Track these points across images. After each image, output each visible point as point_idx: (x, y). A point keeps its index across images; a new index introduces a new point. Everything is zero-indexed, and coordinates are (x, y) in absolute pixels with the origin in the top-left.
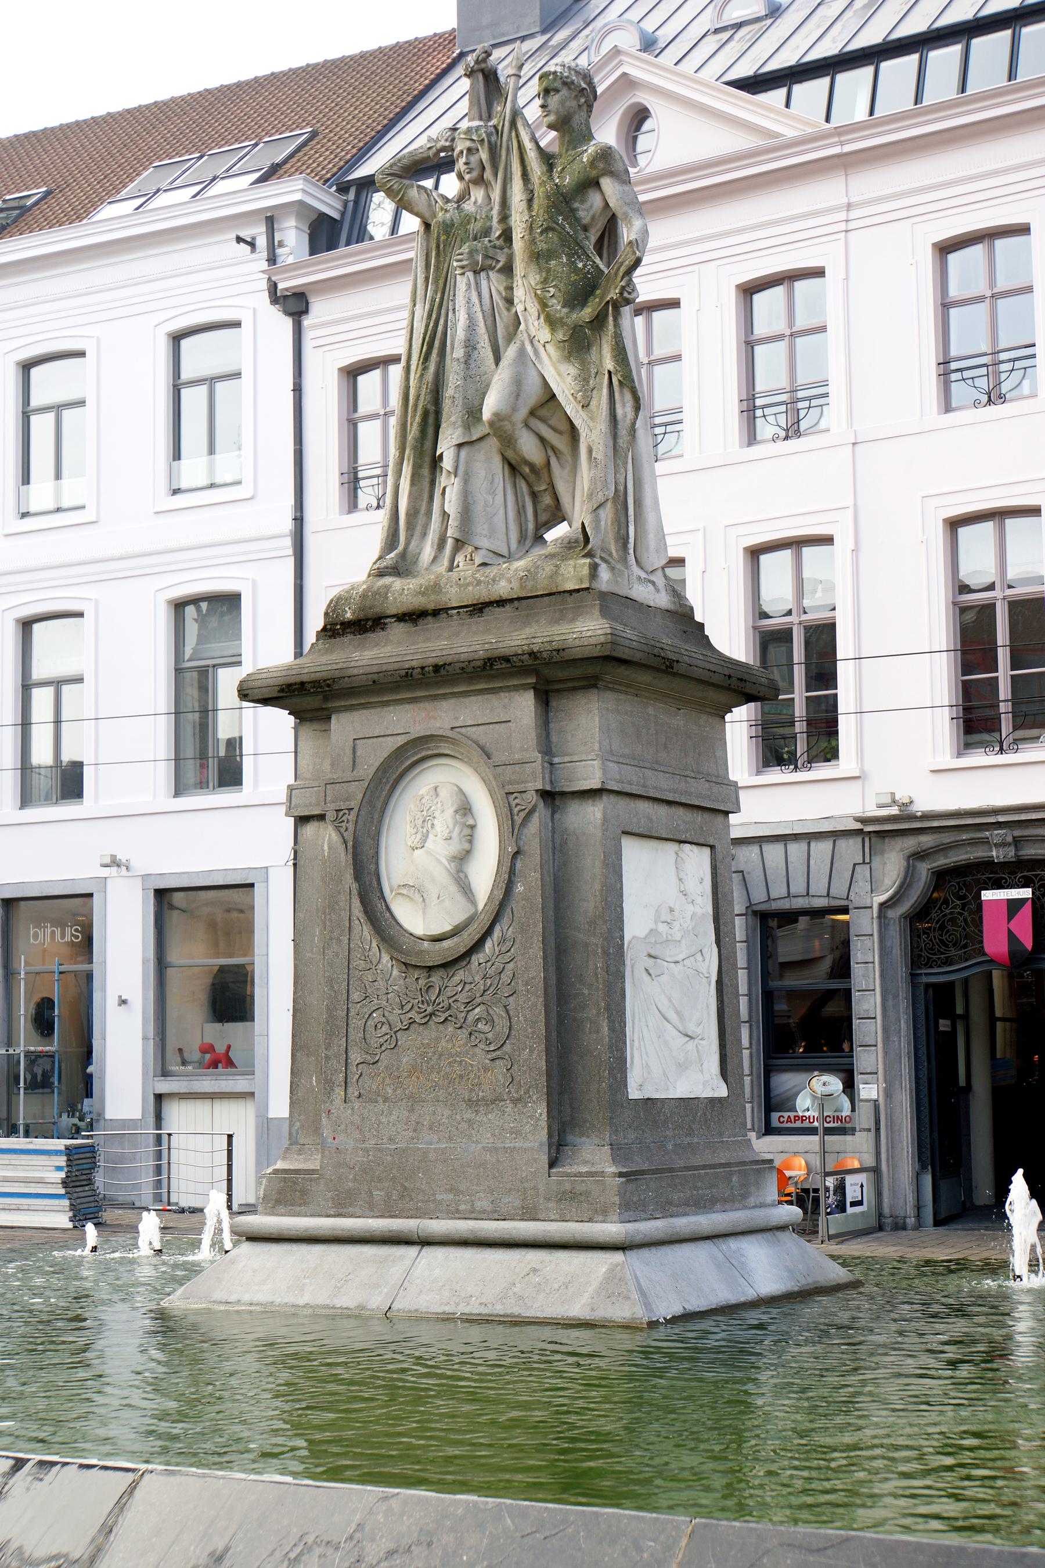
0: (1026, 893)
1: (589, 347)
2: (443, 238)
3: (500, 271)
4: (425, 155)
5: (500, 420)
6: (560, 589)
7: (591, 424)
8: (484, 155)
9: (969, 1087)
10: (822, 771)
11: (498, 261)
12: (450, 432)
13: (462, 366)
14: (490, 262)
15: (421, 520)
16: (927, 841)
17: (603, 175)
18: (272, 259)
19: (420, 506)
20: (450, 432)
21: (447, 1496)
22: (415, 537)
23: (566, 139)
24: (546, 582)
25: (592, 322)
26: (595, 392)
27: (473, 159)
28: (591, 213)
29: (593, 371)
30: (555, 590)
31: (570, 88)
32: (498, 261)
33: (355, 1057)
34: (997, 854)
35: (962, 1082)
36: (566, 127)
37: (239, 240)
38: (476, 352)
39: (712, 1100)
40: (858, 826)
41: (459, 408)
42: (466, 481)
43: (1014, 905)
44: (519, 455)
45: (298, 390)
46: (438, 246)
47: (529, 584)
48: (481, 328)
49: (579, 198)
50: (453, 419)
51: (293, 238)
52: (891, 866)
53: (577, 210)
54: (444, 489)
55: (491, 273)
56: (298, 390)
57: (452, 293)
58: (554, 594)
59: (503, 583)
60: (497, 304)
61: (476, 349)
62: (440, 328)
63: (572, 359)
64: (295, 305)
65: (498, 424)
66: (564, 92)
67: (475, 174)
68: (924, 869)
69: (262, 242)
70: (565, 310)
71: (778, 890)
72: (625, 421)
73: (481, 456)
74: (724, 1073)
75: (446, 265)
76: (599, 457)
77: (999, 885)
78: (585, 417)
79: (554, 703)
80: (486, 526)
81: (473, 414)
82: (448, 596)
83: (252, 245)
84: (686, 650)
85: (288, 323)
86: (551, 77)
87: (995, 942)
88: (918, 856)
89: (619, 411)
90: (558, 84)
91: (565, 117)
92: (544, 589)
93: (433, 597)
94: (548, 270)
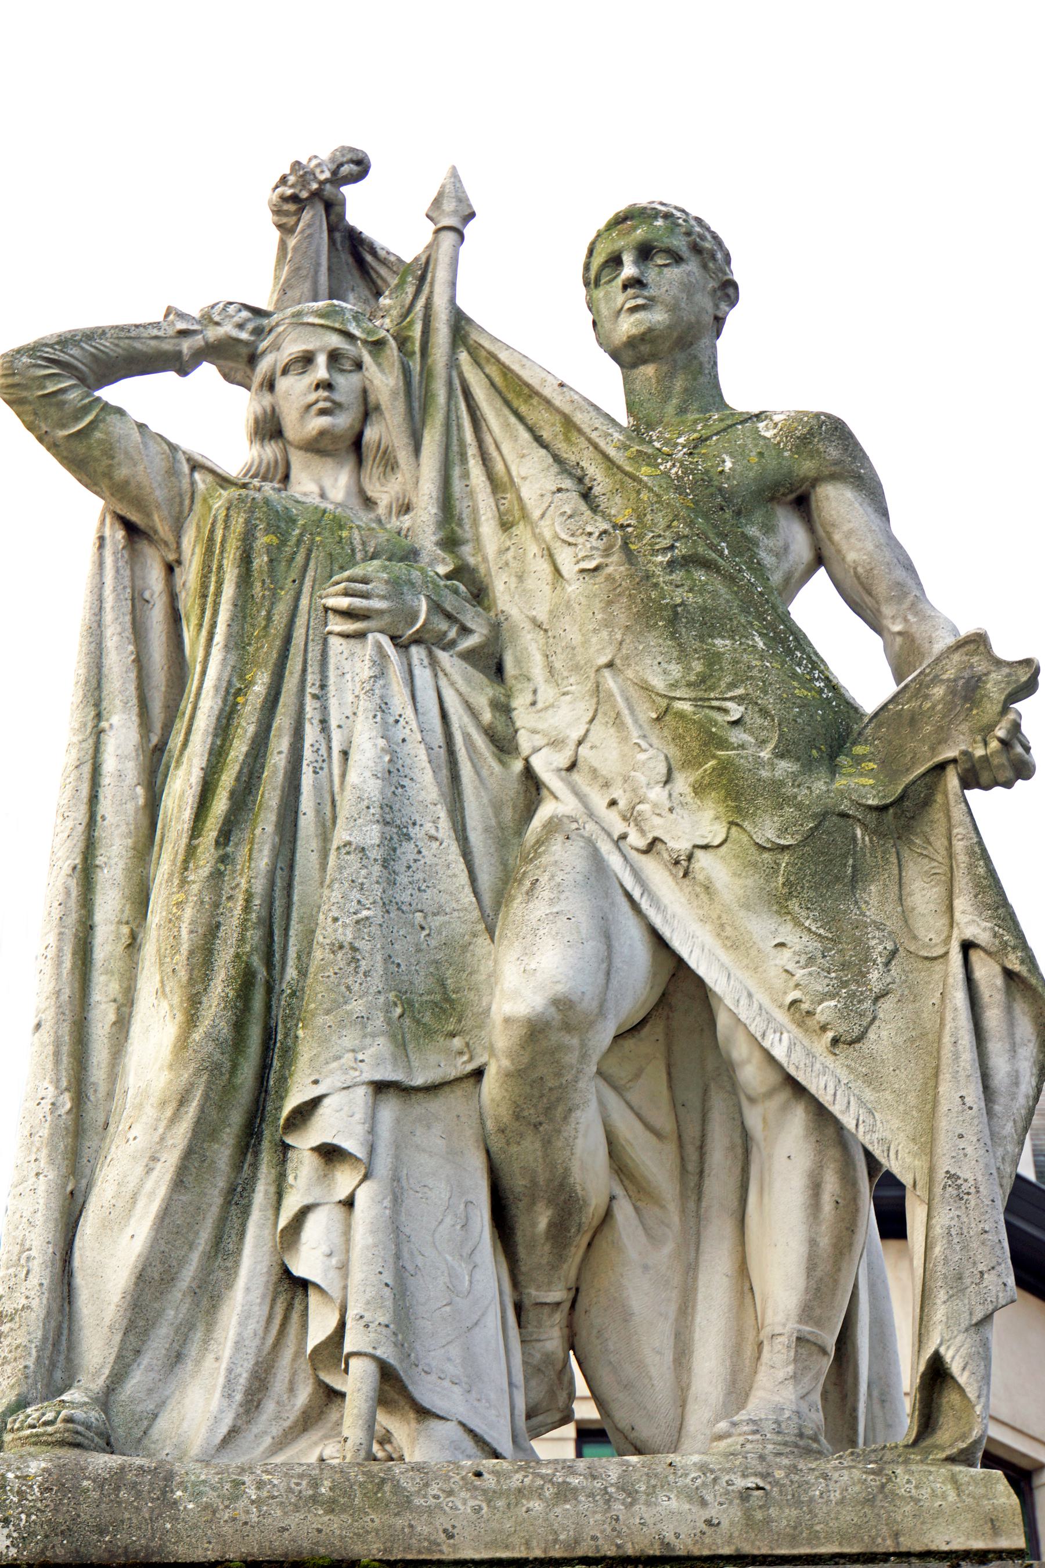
1: (856, 881)
2: (263, 540)
3: (468, 656)
4: (167, 346)
5: (567, 1027)
6: (907, 1544)
7: (868, 1095)
8: (383, 380)
11: (465, 631)
12: (348, 1042)
13: (377, 869)
14: (443, 625)
15: (175, 1307)
17: (833, 477)
19: (182, 1262)
20: (348, 1042)
22: (145, 1360)
23: (679, 384)
24: (849, 1516)
25: (882, 809)
26: (887, 1005)
27: (347, 384)
28: (785, 566)
29: (879, 949)
30: (888, 1545)
31: (705, 267)
32: (465, 631)
36: (681, 357)
38: (409, 847)
41: (376, 982)
42: (397, 1195)
44: (552, 1166)
46: (246, 560)
47: (783, 1517)
48: (426, 785)
49: (758, 516)
50: (357, 1006)
53: (753, 542)
54: (305, 1212)
55: (443, 656)
57: (312, 677)
58: (885, 1557)
59: (671, 1503)
60: (467, 737)
61: (408, 838)
62: (278, 759)
63: (794, 905)
65: (556, 1037)
66: (692, 266)
67: (343, 421)
70: (785, 767)
72: (1013, 1097)
73: (433, 1139)
75: (281, 610)
76: (965, 1173)
78: (844, 1076)
80: (454, 1351)
81: (431, 1004)
82: (442, 1522)
86: (659, 222)
89: (1000, 1065)
90: (679, 243)
91: (690, 327)
92: (843, 1537)
93: (375, 1519)
94: (713, 659)
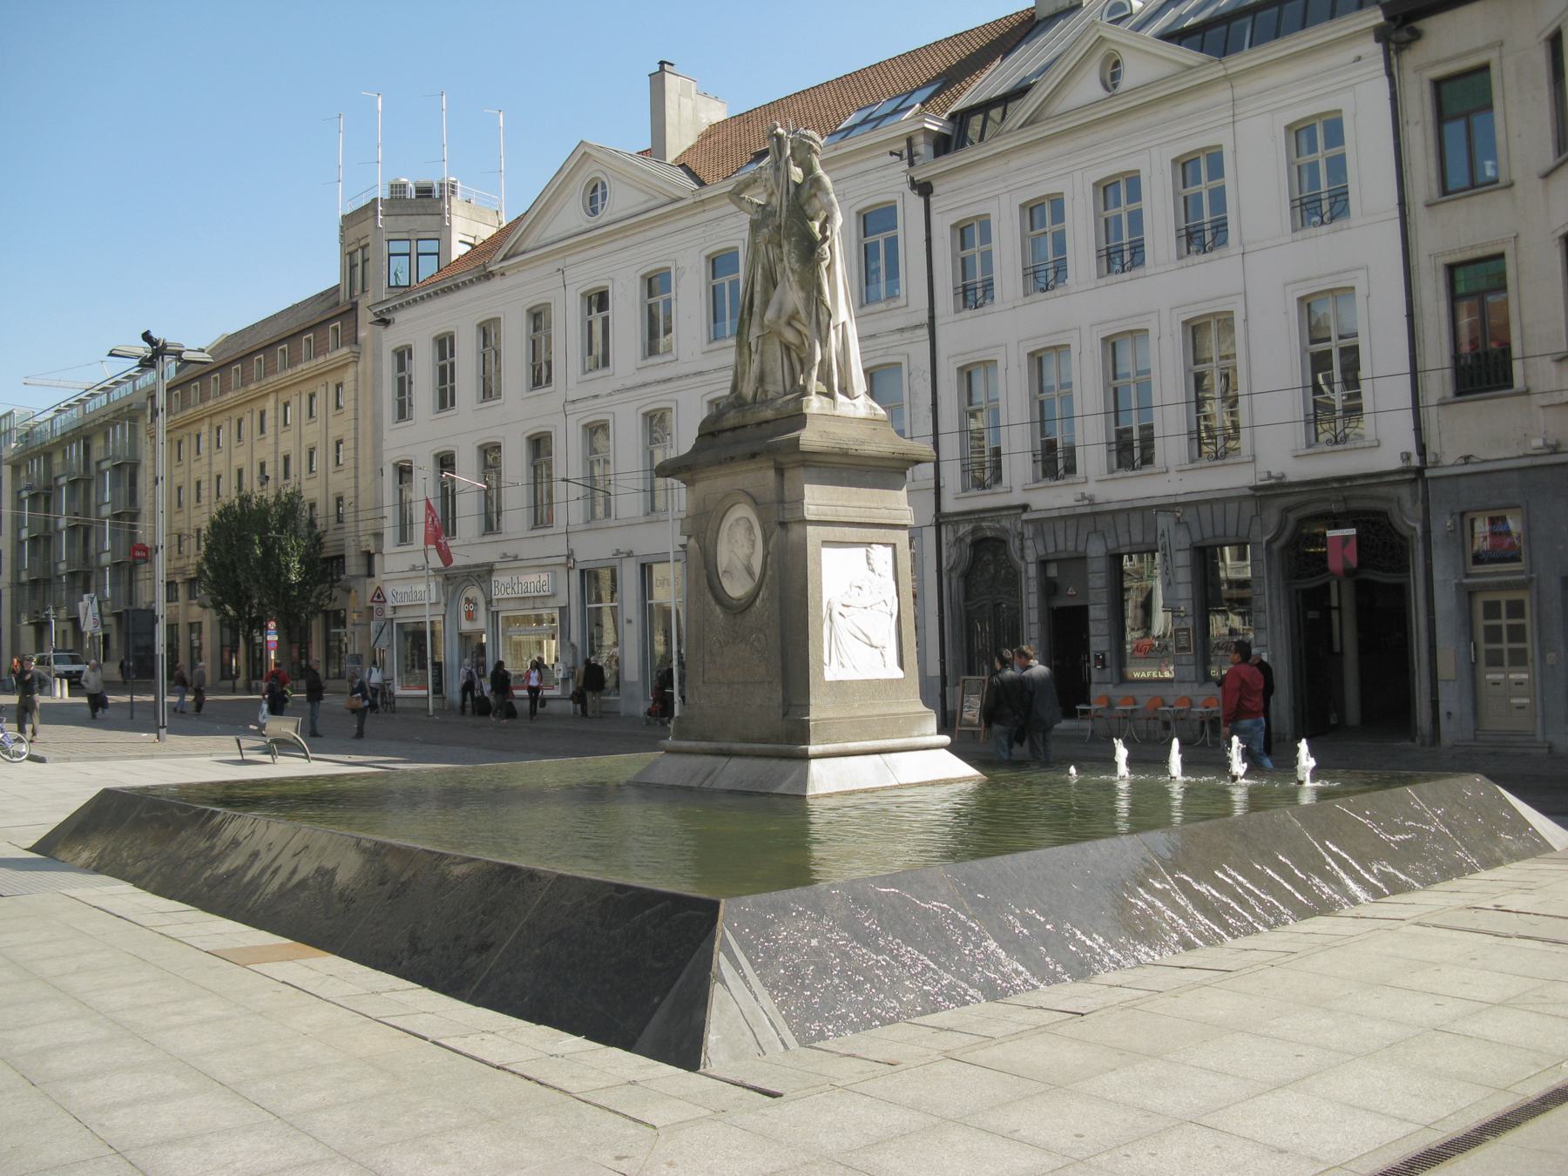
0: (1352, 532)
9: (1342, 653)
10: (1147, 470)
16: (1293, 500)
18: (911, 164)
21: (578, 874)
33: (707, 658)
34: (1333, 507)
35: (1337, 648)
37: (892, 153)
39: (891, 681)
40: (1250, 492)
43: (1346, 538)
45: (929, 240)
51: (922, 147)
52: (1272, 517)
56: (929, 240)
64: (924, 189)
68: (1292, 517)
69: (905, 153)
71: (1208, 532)
74: (901, 665)
77: (1337, 527)
79: (787, 475)
83: (900, 155)
84: (687, 476)
85: (922, 200)
87: (1335, 564)
88: (1287, 510)
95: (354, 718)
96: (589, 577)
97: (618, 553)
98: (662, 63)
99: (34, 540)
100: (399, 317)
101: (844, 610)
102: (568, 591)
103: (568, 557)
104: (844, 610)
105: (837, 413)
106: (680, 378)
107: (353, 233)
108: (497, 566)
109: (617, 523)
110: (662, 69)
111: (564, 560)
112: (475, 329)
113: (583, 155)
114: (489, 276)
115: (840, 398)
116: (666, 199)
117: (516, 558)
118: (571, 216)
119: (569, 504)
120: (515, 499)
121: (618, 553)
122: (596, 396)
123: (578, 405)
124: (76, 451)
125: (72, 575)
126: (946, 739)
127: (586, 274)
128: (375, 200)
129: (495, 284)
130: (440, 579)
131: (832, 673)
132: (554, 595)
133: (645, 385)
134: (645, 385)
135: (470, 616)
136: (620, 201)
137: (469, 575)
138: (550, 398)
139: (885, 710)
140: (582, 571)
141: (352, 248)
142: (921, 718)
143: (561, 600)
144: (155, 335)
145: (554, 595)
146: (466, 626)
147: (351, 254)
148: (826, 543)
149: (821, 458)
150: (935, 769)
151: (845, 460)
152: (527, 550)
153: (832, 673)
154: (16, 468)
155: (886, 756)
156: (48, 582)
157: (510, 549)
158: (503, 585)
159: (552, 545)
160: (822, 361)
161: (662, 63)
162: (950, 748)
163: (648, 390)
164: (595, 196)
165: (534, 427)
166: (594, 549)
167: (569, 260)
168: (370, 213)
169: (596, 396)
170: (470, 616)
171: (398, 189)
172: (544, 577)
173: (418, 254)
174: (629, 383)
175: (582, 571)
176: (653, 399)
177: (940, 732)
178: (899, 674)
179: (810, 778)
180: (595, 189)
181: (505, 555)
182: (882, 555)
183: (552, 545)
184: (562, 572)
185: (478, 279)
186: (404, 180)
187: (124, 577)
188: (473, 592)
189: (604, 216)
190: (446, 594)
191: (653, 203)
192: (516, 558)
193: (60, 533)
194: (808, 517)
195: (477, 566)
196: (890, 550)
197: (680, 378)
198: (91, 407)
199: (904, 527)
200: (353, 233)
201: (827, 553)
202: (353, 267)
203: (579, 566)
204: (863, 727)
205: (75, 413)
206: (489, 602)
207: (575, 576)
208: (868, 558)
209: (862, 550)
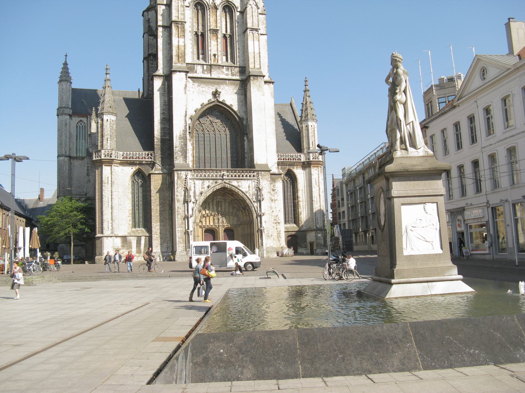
39: (436, 255)
74: (442, 248)
95: (21, 287)
96: (494, 209)
97: (502, 200)
98: (509, 19)
99: (352, 207)
100: (431, 125)
101: (412, 229)
102: (488, 216)
103: (487, 203)
104: (412, 229)
105: (409, 155)
106: (517, 134)
107: (428, 97)
108: (466, 208)
109: (502, 190)
110: (509, 21)
111: (485, 204)
112: (452, 126)
113: (477, 60)
114: (454, 107)
115: (411, 149)
116: (505, 70)
117: (471, 205)
118: (477, 82)
119: (487, 185)
120: (470, 184)
121: (502, 200)
122: (491, 145)
123: (486, 149)
124: (361, 178)
125: (362, 217)
126: (461, 277)
127: (483, 102)
128: (432, 86)
129: (457, 110)
130: (449, 213)
131: (406, 253)
132: (483, 217)
133: (506, 139)
134: (506, 139)
135: (459, 226)
136: (492, 73)
137: (458, 211)
138: (477, 147)
139: (432, 266)
140: (492, 208)
141: (427, 103)
142: (449, 268)
143: (486, 219)
144: (321, 145)
145: (483, 217)
146: (459, 229)
147: (427, 105)
148: (403, 204)
149: (398, 174)
150: (454, 286)
151: (407, 173)
152: (475, 201)
153: (406, 253)
154: (347, 185)
155: (430, 284)
156: (356, 220)
157: (469, 202)
158: (467, 213)
159: (482, 199)
160: (401, 137)
161: (509, 19)
162: (462, 280)
163: (507, 140)
164: (484, 72)
165: (473, 158)
166: (494, 200)
167: (478, 97)
168: (431, 90)
169: (491, 145)
170: (459, 226)
171: (441, 80)
172: (480, 211)
173: (439, 103)
174: (501, 138)
175: (492, 208)
176: (510, 143)
177: (459, 274)
178: (441, 252)
179: (390, 291)
180: (484, 71)
181: (467, 204)
182: (432, 208)
183: (482, 199)
184: (486, 208)
185: (451, 108)
186: (443, 77)
187: (364, 220)
188: (460, 217)
189: (487, 80)
190: (451, 218)
191: (502, 72)
192: (471, 205)
193: (358, 204)
194: (393, 195)
195: (459, 208)
196: (435, 204)
197: (517, 134)
198: (365, 163)
199: (442, 195)
200: (428, 97)
201: (403, 208)
202: (428, 109)
203: (491, 206)
204: (420, 272)
205: (361, 166)
206: (464, 221)
207: (490, 209)
208: (424, 208)
209: (422, 205)
